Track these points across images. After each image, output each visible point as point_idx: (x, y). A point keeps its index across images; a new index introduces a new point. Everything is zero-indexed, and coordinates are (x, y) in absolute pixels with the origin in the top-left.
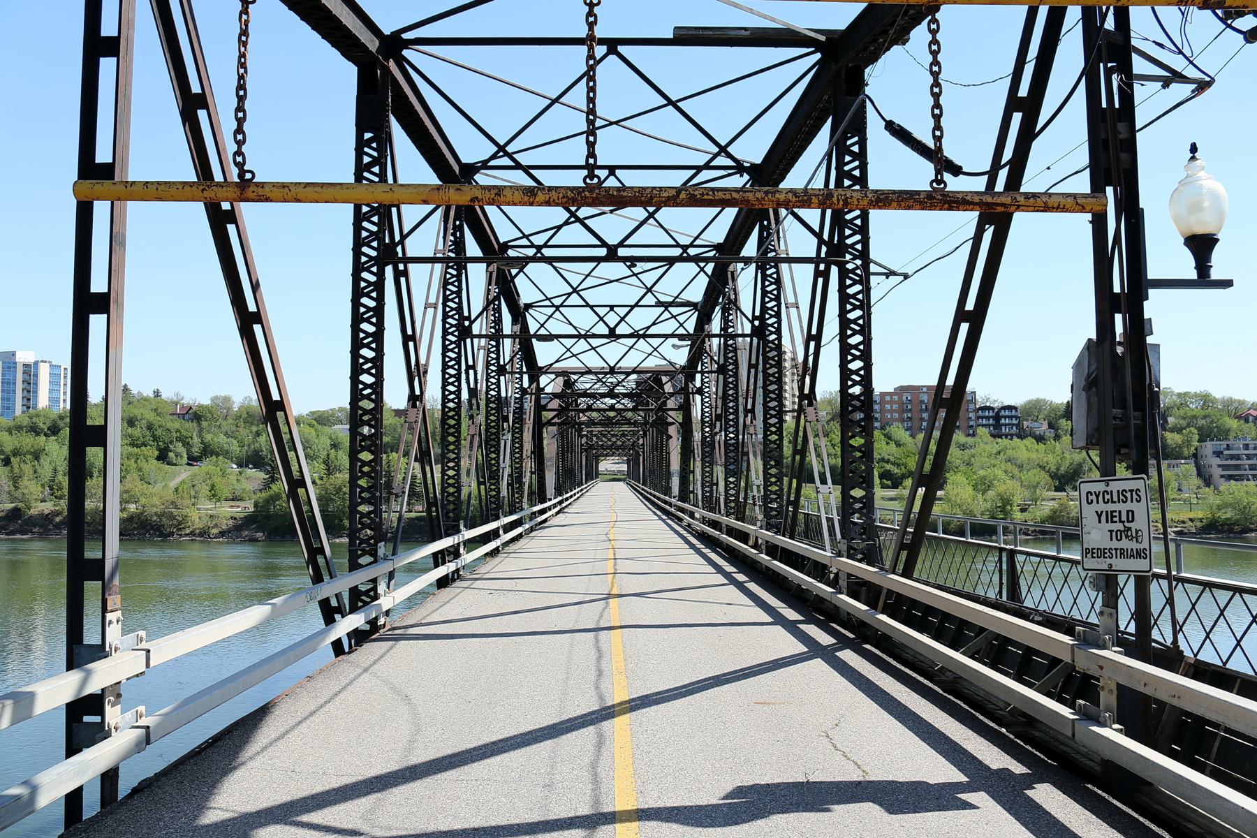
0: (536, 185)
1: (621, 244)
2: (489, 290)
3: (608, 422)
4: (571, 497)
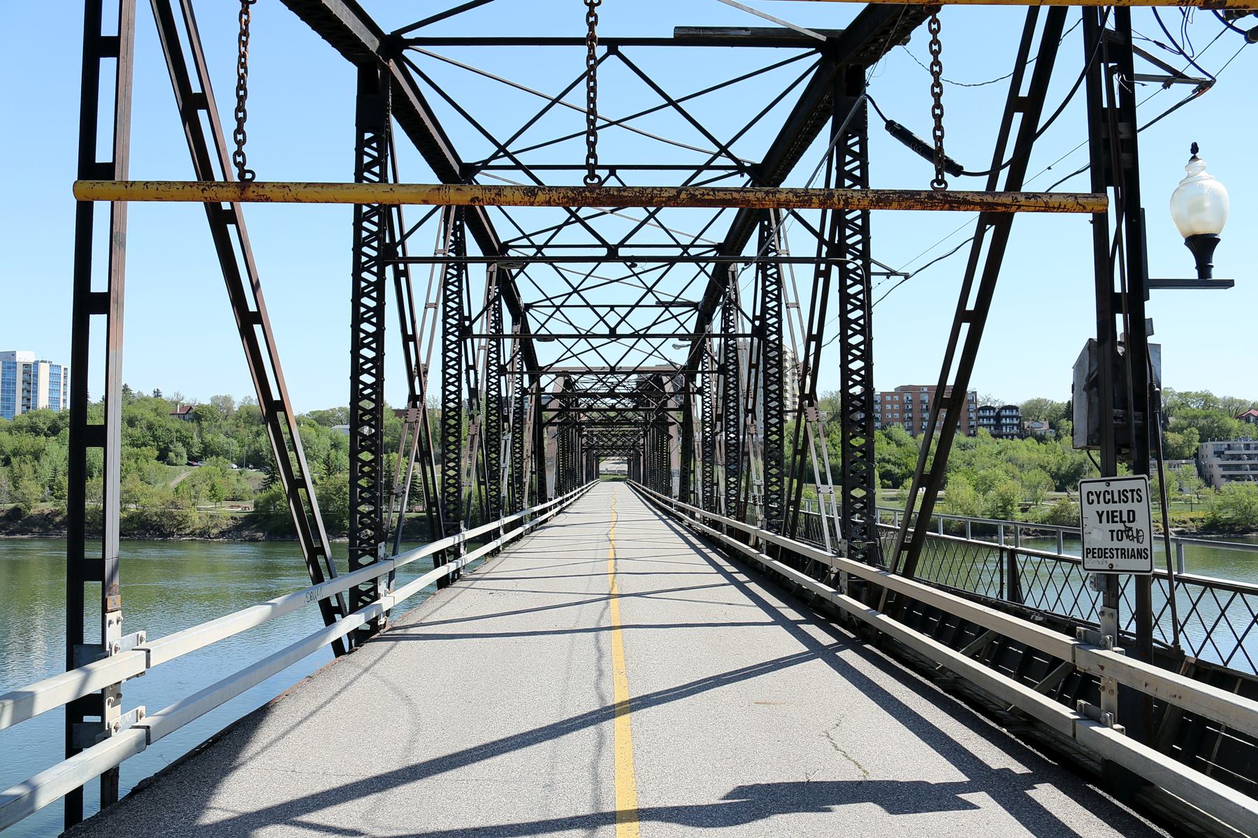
0: (536, 185)
1: (622, 244)
2: (489, 290)
3: (608, 422)
4: (571, 497)
